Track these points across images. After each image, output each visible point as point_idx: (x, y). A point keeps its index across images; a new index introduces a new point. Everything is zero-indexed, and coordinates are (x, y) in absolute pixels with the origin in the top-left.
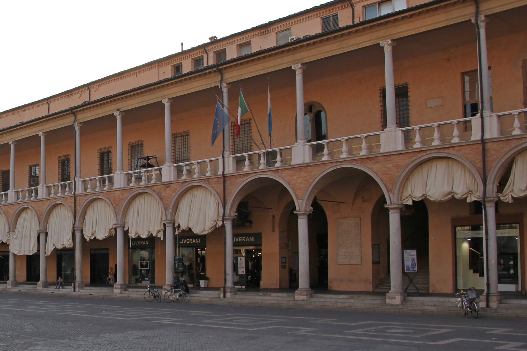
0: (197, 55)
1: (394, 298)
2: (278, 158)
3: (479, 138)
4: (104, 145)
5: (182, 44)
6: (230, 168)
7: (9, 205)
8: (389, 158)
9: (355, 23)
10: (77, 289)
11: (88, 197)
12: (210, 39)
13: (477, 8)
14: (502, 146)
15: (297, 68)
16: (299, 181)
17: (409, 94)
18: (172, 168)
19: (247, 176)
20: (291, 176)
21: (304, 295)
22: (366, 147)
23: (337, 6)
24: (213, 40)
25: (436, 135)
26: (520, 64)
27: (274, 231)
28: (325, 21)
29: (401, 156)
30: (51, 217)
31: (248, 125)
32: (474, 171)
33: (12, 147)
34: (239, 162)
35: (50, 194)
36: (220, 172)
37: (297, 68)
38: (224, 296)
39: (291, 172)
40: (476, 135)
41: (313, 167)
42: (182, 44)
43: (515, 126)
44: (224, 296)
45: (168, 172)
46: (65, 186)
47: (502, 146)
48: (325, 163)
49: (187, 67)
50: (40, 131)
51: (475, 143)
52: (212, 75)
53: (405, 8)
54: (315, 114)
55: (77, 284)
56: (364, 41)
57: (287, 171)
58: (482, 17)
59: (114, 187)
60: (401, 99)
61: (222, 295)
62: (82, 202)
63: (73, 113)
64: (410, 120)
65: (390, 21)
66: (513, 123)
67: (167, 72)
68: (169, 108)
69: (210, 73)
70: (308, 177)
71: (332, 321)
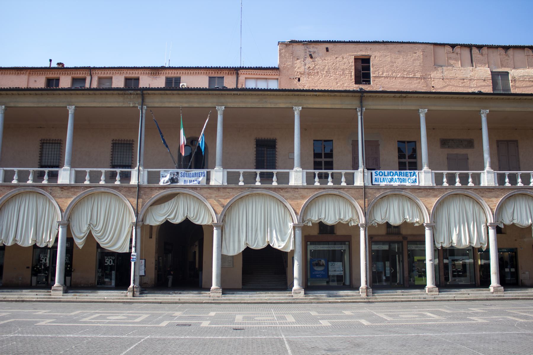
0: (79, 75)
1: (300, 293)
3: (137, 184)
5: (51, 61)
8: (297, 190)
9: (92, 87)
12: (58, 64)
14: (375, 191)
17: (277, 146)
19: (164, 189)
20: (210, 194)
22: (89, 179)
23: (225, 72)
24: (60, 66)
26: (351, 142)
27: (151, 237)
29: (306, 190)
31: (59, 145)
39: (209, 191)
41: (231, 190)
42: (51, 61)
47: (375, 191)
49: (65, 82)
51: (133, 187)
52: (132, 96)
56: (282, 103)
57: (205, 190)
60: (268, 149)
64: (277, 165)
67: (40, 82)
68: (222, 116)
71: (49, 312)
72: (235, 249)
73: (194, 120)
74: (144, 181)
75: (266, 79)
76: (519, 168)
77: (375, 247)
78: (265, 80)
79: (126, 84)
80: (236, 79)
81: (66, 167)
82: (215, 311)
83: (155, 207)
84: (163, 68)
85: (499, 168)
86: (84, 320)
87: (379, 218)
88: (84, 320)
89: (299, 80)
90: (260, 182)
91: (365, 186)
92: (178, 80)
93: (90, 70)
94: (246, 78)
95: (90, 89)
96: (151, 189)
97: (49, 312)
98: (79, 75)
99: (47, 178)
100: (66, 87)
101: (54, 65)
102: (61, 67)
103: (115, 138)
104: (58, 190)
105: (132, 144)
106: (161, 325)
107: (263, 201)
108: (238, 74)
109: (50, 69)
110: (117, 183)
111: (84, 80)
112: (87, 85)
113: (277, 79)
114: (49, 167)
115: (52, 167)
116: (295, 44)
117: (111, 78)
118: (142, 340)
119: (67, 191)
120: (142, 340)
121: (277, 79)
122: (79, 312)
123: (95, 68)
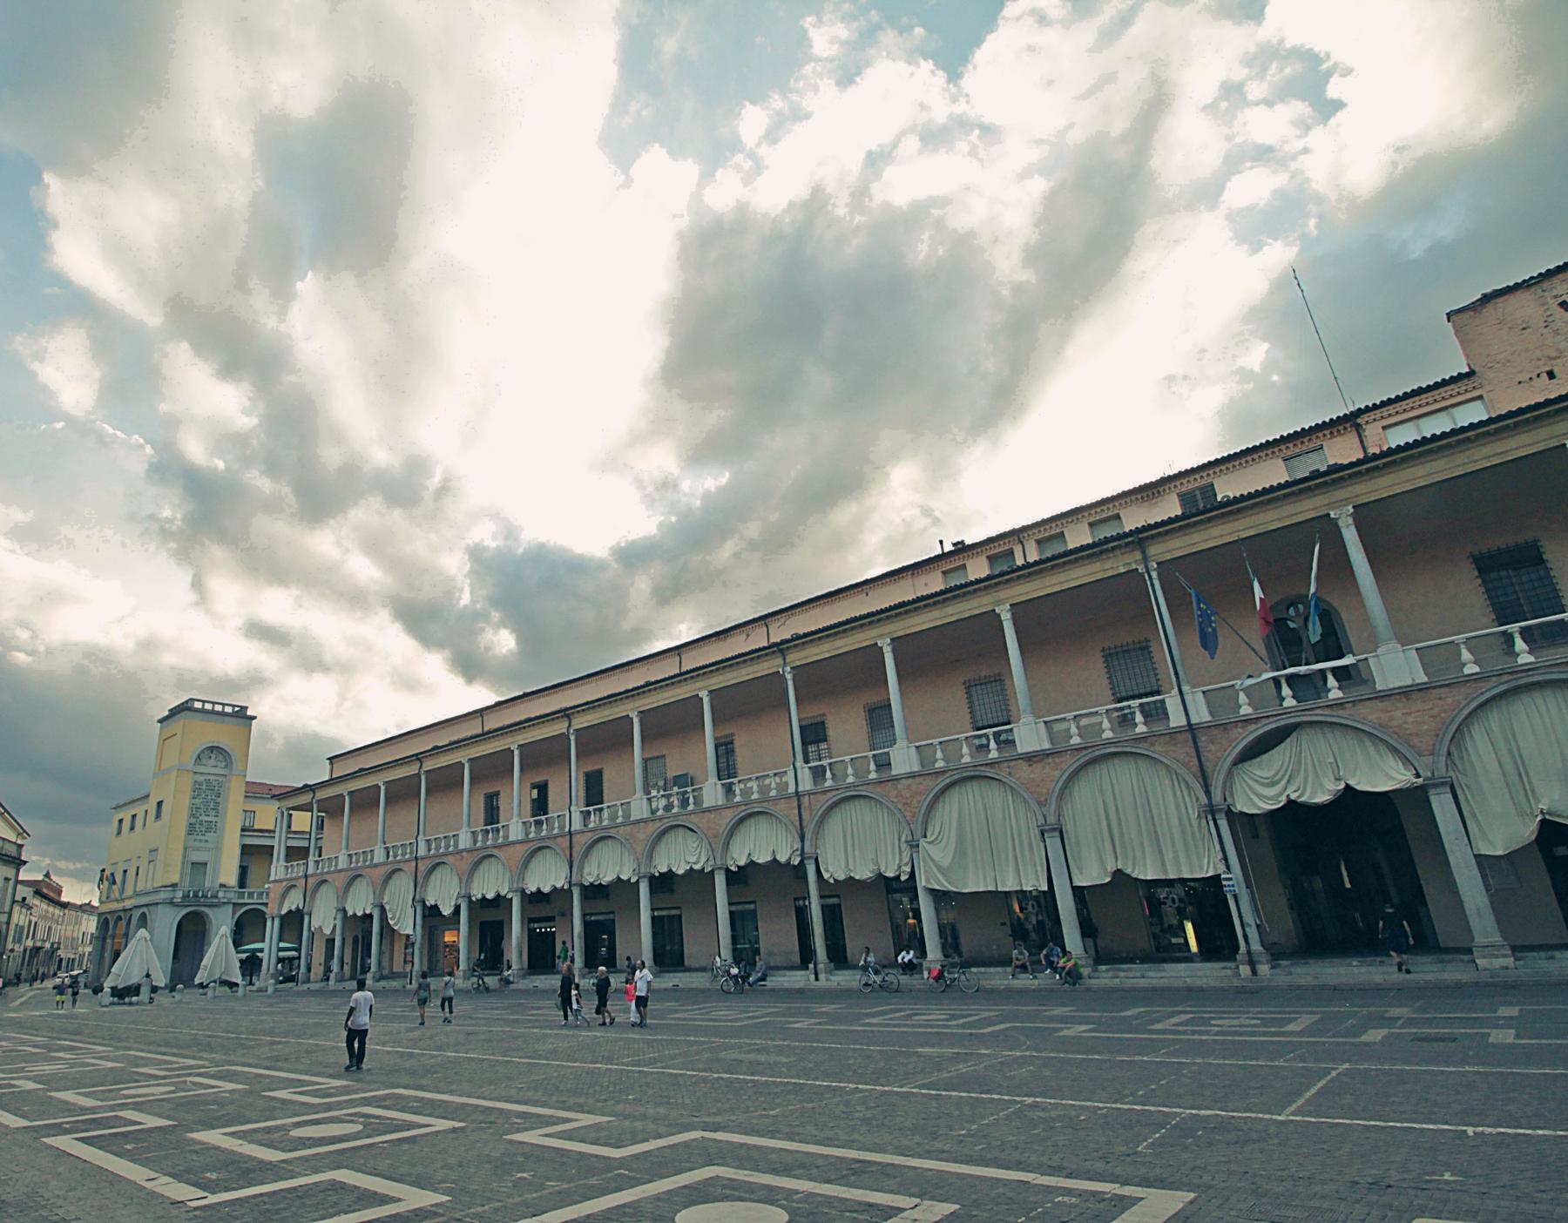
2: (828, 774)
3: (1184, 722)
4: (873, 698)
6: (806, 784)
7: (376, 866)
10: (822, 976)
11: (829, 795)
13: (1143, 552)
15: (704, 694)
16: (1410, 719)
18: (719, 787)
21: (1505, 956)
25: (939, 754)
27: (1256, 836)
28: (1185, 499)
30: (658, 848)
32: (1182, 770)
33: (516, 753)
34: (818, 773)
35: (475, 842)
36: (792, 789)
37: (704, 694)
38: (1254, 972)
40: (1176, 719)
43: (1517, 649)
44: (1254, 972)
45: (712, 793)
46: (487, 832)
48: (737, 805)
50: (784, 667)
51: (1179, 731)
52: (1118, 552)
53: (1485, 418)
54: (725, 749)
55: (821, 966)
56: (1117, 565)
57: (1368, 703)
58: (788, 669)
59: (1172, 724)
61: (813, 977)
62: (582, 841)
63: (781, 651)
65: (1360, 472)
66: (1460, 654)
69: (1114, 548)
70: (1436, 710)
71: (775, 1014)
72: (1505, 830)
73: (1280, 553)
74: (1201, 714)
75: (1445, 408)
76: (1340, 648)
77: (734, 908)
78: (1443, 414)
79: (1183, 504)
80: (1357, 439)
81: (1026, 719)
82: (1518, 1003)
83: (1246, 765)
84: (1165, 481)
85: (1498, 619)
86: (1159, 1026)
87: (477, 894)
88: (1159, 1026)
89: (1551, 375)
90: (1145, 723)
91: (1189, 724)
92: (1209, 490)
93: (1017, 534)
94: (1384, 428)
95: (1028, 565)
96: (1224, 727)
97: (775, 1014)
98: (999, 546)
99: (1336, 684)
100: (983, 575)
101: (948, 548)
102: (961, 548)
103: (1107, 645)
104: (1023, 764)
105: (1148, 647)
106: (1364, 1038)
107: (1105, 771)
108: (1358, 427)
109: (944, 556)
110: (1141, 729)
111: (1011, 553)
112: (1020, 562)
113: (1480, 397)
114: (1140, 696)
115: (1146, 695)
116: (1500, 302)
117: (1062, 534)
118: (1334, 1073)
119: (1039, 765)
120: (1334, 1073)
121: (1480, 397)
122: (1137, 1010)
123: (1025, 529)
